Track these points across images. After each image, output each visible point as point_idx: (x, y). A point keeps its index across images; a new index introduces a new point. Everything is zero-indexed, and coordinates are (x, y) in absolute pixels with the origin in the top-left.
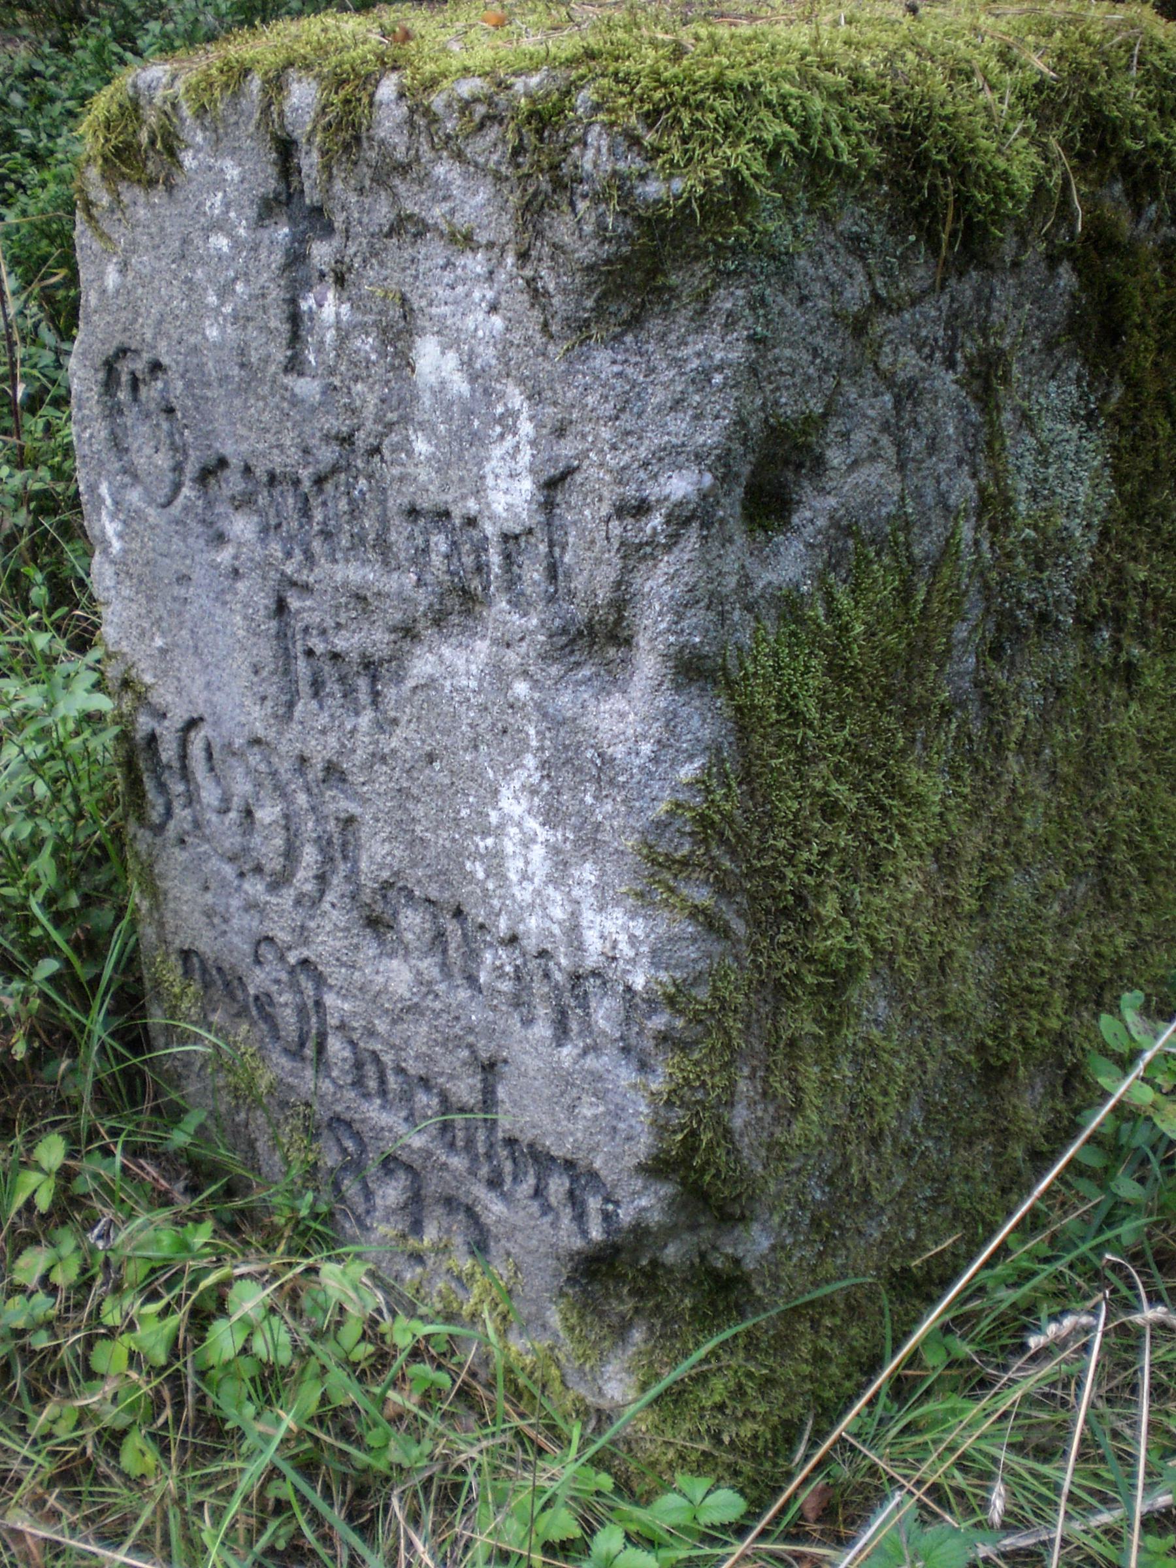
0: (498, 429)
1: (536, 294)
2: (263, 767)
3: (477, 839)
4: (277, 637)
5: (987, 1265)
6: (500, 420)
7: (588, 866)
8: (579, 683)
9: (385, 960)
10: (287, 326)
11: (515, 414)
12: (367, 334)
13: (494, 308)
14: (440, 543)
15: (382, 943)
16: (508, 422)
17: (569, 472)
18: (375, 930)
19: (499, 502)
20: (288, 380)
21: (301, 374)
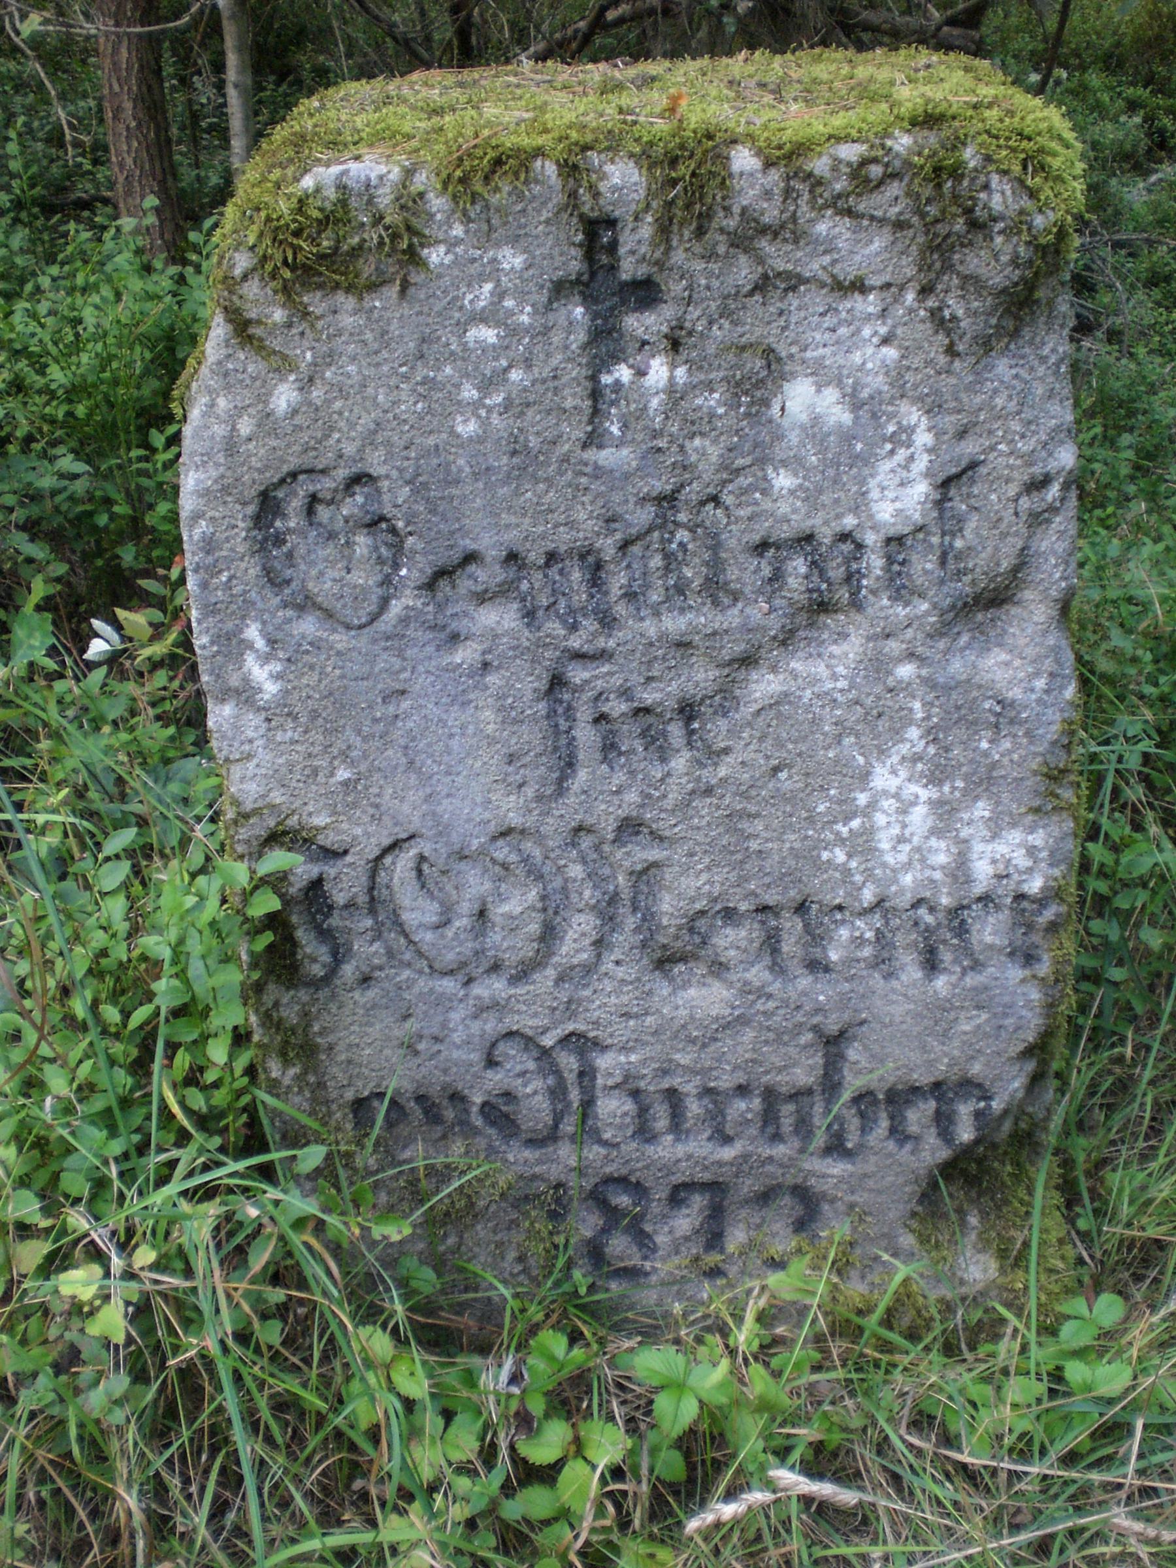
0: (888, 446)
1: (940, 321)
2: (513, 858)
3: (839, 827)
4: (548, 717)
5: (167, 1319)
6: (892, 438)
7: (980, 804)
8: (962, 650)
9: (681, 993)
10: (588, 403)
11: (911, 430)
12: (712, 391)
13: (885, 341)
14: (798, 565)
15: (671, 980)
16: (902, 437)
17: (973, 465)
18: (663, 971)
19: (884, 512)
20: (591, 455)
21: (601, 447)
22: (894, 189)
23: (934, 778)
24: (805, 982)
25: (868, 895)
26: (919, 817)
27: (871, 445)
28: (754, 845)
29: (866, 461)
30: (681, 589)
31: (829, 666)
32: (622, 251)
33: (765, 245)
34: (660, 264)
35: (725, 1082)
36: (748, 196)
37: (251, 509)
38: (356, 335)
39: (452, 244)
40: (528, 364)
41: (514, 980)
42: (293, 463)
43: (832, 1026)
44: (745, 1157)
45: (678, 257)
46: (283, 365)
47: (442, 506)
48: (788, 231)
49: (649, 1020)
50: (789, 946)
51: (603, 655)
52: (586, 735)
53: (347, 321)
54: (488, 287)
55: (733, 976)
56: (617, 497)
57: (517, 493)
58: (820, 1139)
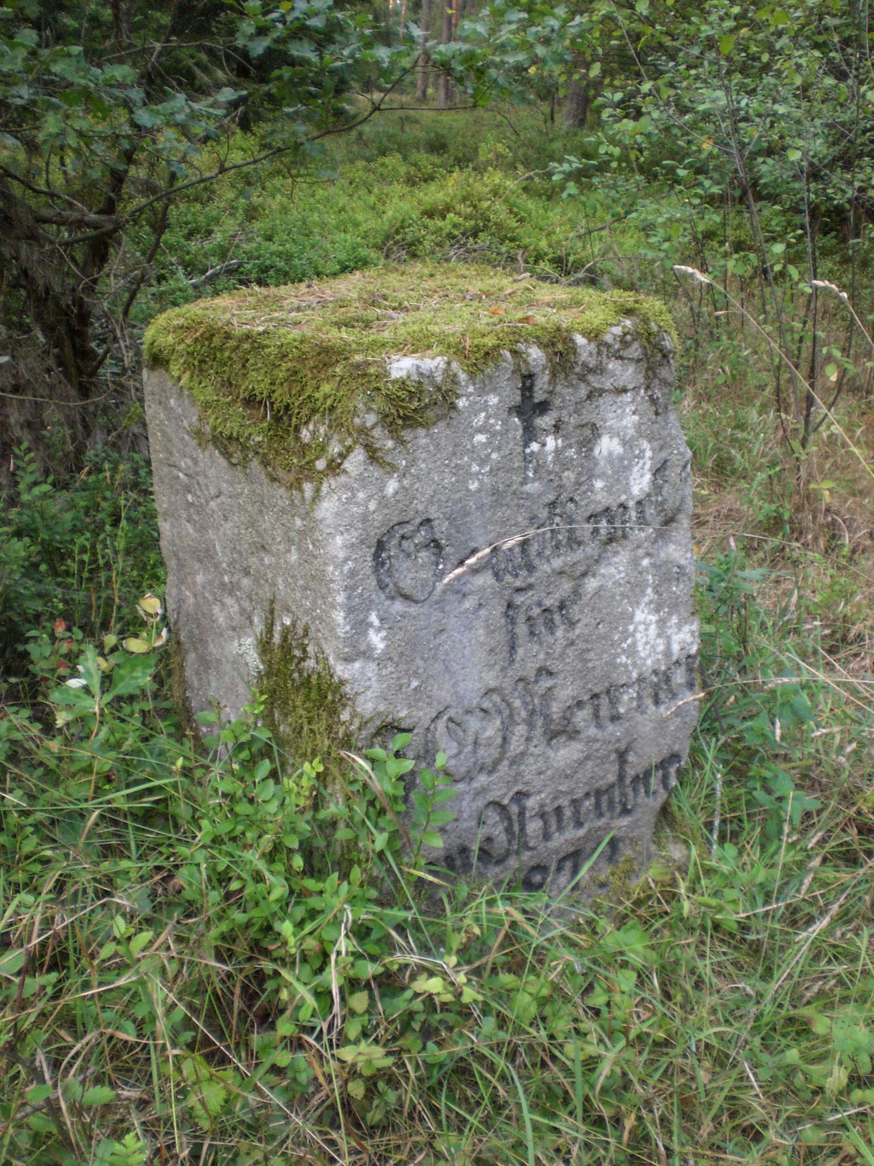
11: (643, 451)
14: (604, 524)
17: (666, 461)
22: (636, 345)
23: (657, 611)
24: (611, 728)
25: (635, 675)
26: (653, 630)
27: (630, 461)
28: (590, 665)
29: (628, 469)
30: (557, 547)
31: (615, 568)
32: (536, 388)
33: (591, 378)
34: (551, 392)
35: (579, 794)
36: (584, 356)
37: (373, 550)
38: (425, 448)
39: (468, 396)
40: (499, 449)
41: (490, 773)
42: (396, 520)
43: (623, 746)
44: (589, 831)
45: (559, 388)
46: (393, 468)
47: (462, 528)
48: (599, 370)
49: (549, 772)
50: (604, 712)
51: (530, 587)
52: (522, 629)
53: (423, 441)
54: (483, 414)
55: (582, 736)
56: (535, 507)
57: (494, 514)
58: (618, 808)
